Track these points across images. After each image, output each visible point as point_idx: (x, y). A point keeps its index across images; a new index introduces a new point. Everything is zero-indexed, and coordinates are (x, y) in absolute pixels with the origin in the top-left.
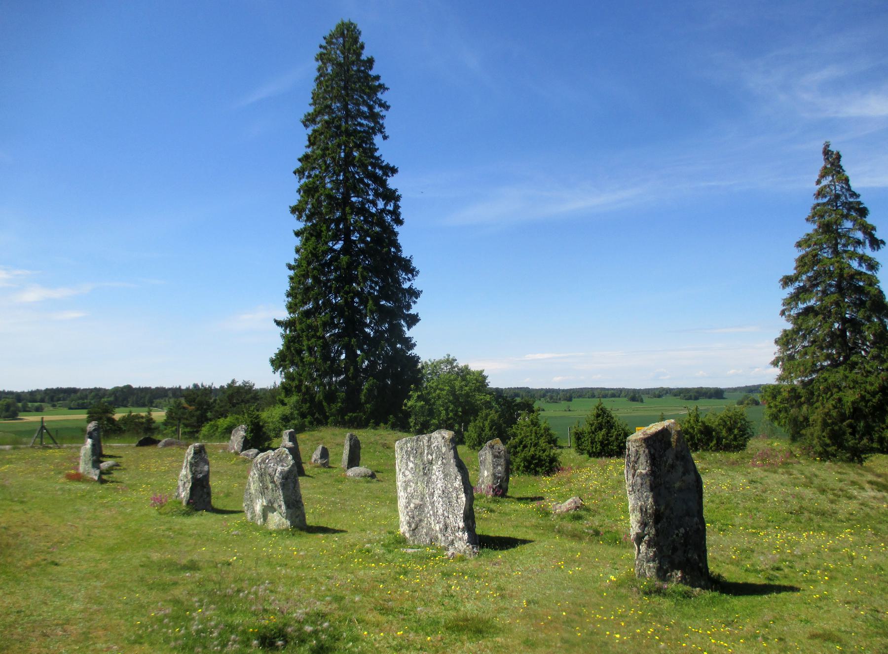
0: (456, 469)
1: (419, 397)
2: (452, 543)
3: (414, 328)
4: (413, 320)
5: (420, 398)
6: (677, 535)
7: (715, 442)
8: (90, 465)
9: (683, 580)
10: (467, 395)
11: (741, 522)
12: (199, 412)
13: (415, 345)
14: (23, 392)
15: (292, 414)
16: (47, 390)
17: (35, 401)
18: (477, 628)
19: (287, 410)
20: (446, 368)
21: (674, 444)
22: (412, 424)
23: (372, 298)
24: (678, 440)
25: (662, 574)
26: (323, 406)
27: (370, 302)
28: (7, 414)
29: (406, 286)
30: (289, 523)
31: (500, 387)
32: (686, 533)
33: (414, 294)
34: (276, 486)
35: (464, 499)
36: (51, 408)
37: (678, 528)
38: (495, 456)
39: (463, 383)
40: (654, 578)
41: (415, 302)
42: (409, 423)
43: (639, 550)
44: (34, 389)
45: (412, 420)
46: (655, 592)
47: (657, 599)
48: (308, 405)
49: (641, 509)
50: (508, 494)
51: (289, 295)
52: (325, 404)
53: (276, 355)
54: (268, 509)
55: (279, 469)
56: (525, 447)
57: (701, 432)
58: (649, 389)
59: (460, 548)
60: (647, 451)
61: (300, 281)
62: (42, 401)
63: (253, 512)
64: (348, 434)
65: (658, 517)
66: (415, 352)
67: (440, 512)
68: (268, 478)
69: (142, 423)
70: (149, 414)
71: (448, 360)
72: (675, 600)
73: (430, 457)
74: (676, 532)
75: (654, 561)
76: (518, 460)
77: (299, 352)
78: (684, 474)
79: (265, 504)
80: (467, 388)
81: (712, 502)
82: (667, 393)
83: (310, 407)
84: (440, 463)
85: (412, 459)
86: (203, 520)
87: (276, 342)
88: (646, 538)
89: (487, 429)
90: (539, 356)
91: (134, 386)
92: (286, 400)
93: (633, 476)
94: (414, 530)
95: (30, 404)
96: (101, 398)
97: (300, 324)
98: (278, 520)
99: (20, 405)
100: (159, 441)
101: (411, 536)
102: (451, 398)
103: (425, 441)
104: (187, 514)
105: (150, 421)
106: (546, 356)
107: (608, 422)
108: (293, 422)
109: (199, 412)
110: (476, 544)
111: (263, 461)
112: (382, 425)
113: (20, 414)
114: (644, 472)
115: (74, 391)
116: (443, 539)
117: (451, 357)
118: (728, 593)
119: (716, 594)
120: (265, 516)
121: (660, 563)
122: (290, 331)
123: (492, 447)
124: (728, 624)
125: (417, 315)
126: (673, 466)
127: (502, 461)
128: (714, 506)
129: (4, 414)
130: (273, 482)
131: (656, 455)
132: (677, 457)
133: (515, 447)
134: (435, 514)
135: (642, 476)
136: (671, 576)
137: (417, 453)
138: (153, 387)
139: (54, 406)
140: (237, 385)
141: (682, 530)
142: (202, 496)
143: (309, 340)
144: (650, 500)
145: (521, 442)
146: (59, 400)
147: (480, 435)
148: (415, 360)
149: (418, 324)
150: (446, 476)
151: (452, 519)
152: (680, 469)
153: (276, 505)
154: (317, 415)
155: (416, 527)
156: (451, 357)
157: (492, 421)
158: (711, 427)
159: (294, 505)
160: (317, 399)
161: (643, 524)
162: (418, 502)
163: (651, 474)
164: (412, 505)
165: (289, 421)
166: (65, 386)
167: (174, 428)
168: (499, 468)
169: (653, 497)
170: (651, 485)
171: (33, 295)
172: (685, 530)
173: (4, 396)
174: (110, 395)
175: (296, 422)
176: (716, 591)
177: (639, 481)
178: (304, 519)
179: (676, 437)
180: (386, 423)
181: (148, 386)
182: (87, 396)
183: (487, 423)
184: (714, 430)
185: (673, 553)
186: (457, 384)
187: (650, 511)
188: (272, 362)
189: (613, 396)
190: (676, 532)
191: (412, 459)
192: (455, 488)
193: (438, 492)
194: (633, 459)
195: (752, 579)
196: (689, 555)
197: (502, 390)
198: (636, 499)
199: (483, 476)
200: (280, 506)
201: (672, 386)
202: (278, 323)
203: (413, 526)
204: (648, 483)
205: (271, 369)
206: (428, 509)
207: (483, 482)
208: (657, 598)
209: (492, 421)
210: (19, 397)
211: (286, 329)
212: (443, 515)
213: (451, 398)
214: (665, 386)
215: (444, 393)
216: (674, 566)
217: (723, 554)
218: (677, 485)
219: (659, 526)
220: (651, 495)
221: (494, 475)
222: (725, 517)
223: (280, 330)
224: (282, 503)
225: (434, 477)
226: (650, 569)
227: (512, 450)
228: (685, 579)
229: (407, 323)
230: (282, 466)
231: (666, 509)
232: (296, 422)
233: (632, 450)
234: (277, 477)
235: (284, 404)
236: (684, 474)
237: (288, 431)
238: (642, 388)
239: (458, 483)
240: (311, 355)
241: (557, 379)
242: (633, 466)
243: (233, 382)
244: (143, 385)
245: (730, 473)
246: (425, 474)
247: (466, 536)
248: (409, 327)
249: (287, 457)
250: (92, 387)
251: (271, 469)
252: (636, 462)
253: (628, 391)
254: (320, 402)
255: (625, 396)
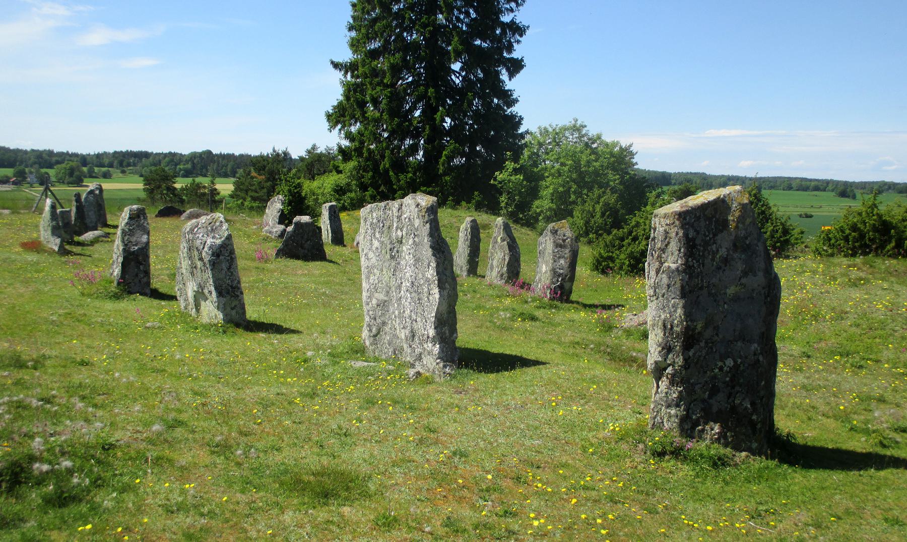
0: (430, 252)
1: (515, 170)
2: (419, 358)
3: (519, 77)
4: (516, 66)
5: (516, 171)
6: (721, 369)
7: (893, 244)
8: (49, 232)
9: (721, 438)
10: (596, 173)
11: (891, 357)
12: (269, 184)
13: (516, 101)
14: (89, 155)
15: (348, 184)
16: (115, 152)
17: (104, 166)
18: (329, 487)
19: (343, 179)
20: (572, 138)
21: (732, 225)
22: (503, 205)
23: (458, 33)
24: (741, 219)
25: (689, 427)
26: (389, 177)
27: (456, 39)
28: (71, 179)
29: (506, 18)
30: (221, 316)
31: (669, 171)
32: (736, 366)
33: (517, 29)
34: (204, 264)
35: (437, 296)
36: (121, 175)
37: (723, 358)
38: (558, 245)
39: (593, 157)
40: (676, 432)
41: (518, 42)
42: (499, 203)
43: (658, 387)
44: (101, 151)
45: (503, 199)
46: (672, 453)
47: (669, 463)
48: (370, 174)
49: (665, 326)
50: (574, 297)
51: (351, 28)
52: (391, 173)
53: (334, 108)
54: (200, 296)
55: (210, 241)
56: (635, 239)
57: (875, 229)
58: (866, 183)
59: (429, 365)
60: (681, 234)
61: (363, 9)
62: (111, 165)
63: (186, 300)
64: (469, 219)
65: (689, 339)
66: (516, 109)
67: (408, 312)
68: (196, 253)
69: (204, 194)
70: (213, 183)
71: (575, 126)
72: (698, 468)
73: (399, 233)
74: (720, 364)
75: (678, 405)
76: (622, 256)
77: (362, 105)
78: (745, 274)
79: (195, 289)
80: (597, 164)
81: (858, 326)
82: (890, 188)
83: (373, 177)
84: (411, 241)
85: (377, 235)
86: (137, 307)
87: (332, 89)
88: (669, 370)
89: (598, 215)
90: (723, 132)
91: (215, 151)
92: (341, 167)
93: (658, 272)
94: (375, 336)
95: (96, 169)
96: (176, 165)
97: (363, 66)
98: (211, 311)
99: (85, 169)
100: (184, 211)
101: (371, 344)
102: (574, 176)
103: (395, 210)
104: (116, 297)
105: (214, 192)
106: (734, 132)
107: (763, 212)
108: (349, 194)
109: (269, 184)
110: (453, 361)
111: (192, 230)
112: (464, 203)
113: (85, 180)
114: (673, 266)
115: (145, 155)
116: (409, 351)
117: (579, 123)
118: (791, 464)
119: (772, 463)
120: (197, 306)
121: (687, 410)
122: (352, 77)
123: (554, 232)
124: (756, 515)
125: (522, 60)
126: (726, 261)
127: (567, 252)
128: (859, 331)
129: (67, 179)
130: (201, 259)
131: (698, 241)
132: (735, 246)
133: (622, 239)
134: (401, 316)
135: (670, 273)
136: (703, 430)
137: (383, 226)
138: (237, 154)
139: (123, 172)
140: (319, 151)
141: (730, 362)
142: (137, 275)
143: (373, 89)
144: (680, 311)
145: (630, 233)
146: (129, 165)
147: (587, 223)
148: (515, 122)
149: (522, 72)
150: (417, 260)
151: (420, 324)
152: (740, 266)
153: (206, 291)
154: (382, 188)
155: (378, 333)
156: (579, 123)
157: (606, 204)
158: (891, 223)
159: (229, 291)
160: (381, 167)
161: (667, 349)
162: (381, 296)
163: (684, 271)
164: (374, 302)
165: (344, 194)
166: (136, 148)
167: (239, 202)
168: (562, 261)
169: (684, 307)
170: (682, 287)
171: (98, 37)
172: (735, 362)
173: (68, 158)
174: (187, 162)
175: (353, 195)
176: (773, 458)
177: (665, 280)
178: (244, 313)
179: (737, 214)
180: (468, 202)
181: (231, 152)
182: (160, 162)
183: (598, 208)
184: (894, 228)
185: (710, 397)
186: (584, 158)
187: (677, 329)
188: (329, 116)
189: (817, 189)
190: (720, 364)
191: (377, 235)
192: (428, 280)
193: (406, 284)
194: (659, 245)
195: (859, 444)
196: (737, 402)
197: (670, 174)
198: (657, 309)
199: (541, 272)
200: (210, 292)
201: (897, 181)
202: (336, 65)
203: (374, 330)
204: (678, 285)
205: (326, 125)
206: (393, 308)
207: (540, 280)
208: (672, 462)
209: (606, 204)
210: (84, 160)
211: (346, 73)
212: (410, 316)
213: (574, 176)
214: (888, 179)
215: (566, 169)
216: (709, 417)
217: (801, 403)
218: (731, 290)
219: (691, 354)
220: (681, 303)
221: (554, 271)
222: (869, 349)
223: (339, 75)
224: (213, 288)
225: (403, 262)
226: (670, 418)
227: (617, 242)
228: (725, 437)
229: (508, 70)
230: (214, 237)
231: (706, 327)
232: (353, 195)
233: (660, 230)
234: (206, 254)
235: (339, 172)
236: (745, 274)
237: (328, 205)
238: (857, 180)
239: (431, 273)
240: (376, 107)
241: (745, 163)
242: (659, 257)
243: (314, 147)
244: (225, 151)
245: (897, 287)
246: (392, 257)
247: (437, 348)
248: (511, 75)
249: (221, 226)
250: (166, 151)
251: (199, 241)
252: (663, 251)
253: (836, 183)
254: (386, 171)
255: (833, 191)
